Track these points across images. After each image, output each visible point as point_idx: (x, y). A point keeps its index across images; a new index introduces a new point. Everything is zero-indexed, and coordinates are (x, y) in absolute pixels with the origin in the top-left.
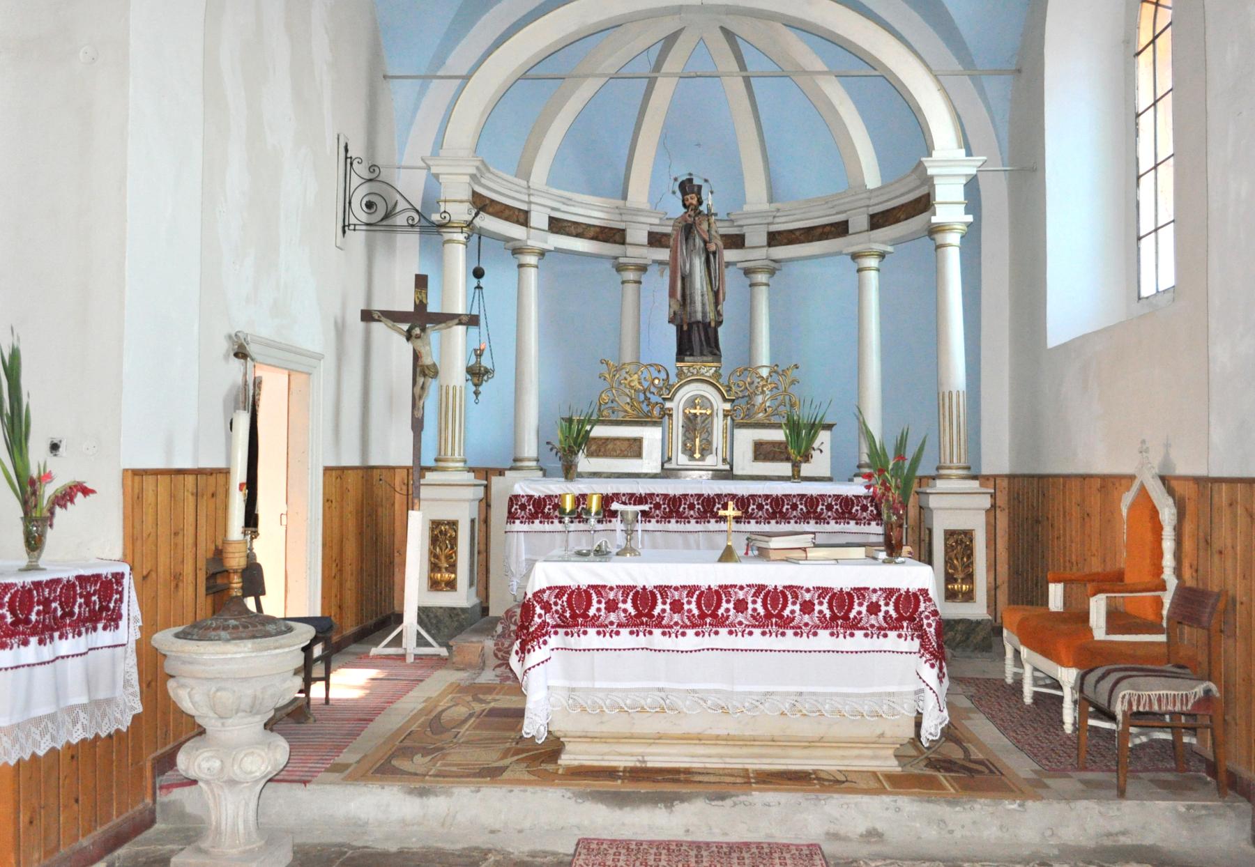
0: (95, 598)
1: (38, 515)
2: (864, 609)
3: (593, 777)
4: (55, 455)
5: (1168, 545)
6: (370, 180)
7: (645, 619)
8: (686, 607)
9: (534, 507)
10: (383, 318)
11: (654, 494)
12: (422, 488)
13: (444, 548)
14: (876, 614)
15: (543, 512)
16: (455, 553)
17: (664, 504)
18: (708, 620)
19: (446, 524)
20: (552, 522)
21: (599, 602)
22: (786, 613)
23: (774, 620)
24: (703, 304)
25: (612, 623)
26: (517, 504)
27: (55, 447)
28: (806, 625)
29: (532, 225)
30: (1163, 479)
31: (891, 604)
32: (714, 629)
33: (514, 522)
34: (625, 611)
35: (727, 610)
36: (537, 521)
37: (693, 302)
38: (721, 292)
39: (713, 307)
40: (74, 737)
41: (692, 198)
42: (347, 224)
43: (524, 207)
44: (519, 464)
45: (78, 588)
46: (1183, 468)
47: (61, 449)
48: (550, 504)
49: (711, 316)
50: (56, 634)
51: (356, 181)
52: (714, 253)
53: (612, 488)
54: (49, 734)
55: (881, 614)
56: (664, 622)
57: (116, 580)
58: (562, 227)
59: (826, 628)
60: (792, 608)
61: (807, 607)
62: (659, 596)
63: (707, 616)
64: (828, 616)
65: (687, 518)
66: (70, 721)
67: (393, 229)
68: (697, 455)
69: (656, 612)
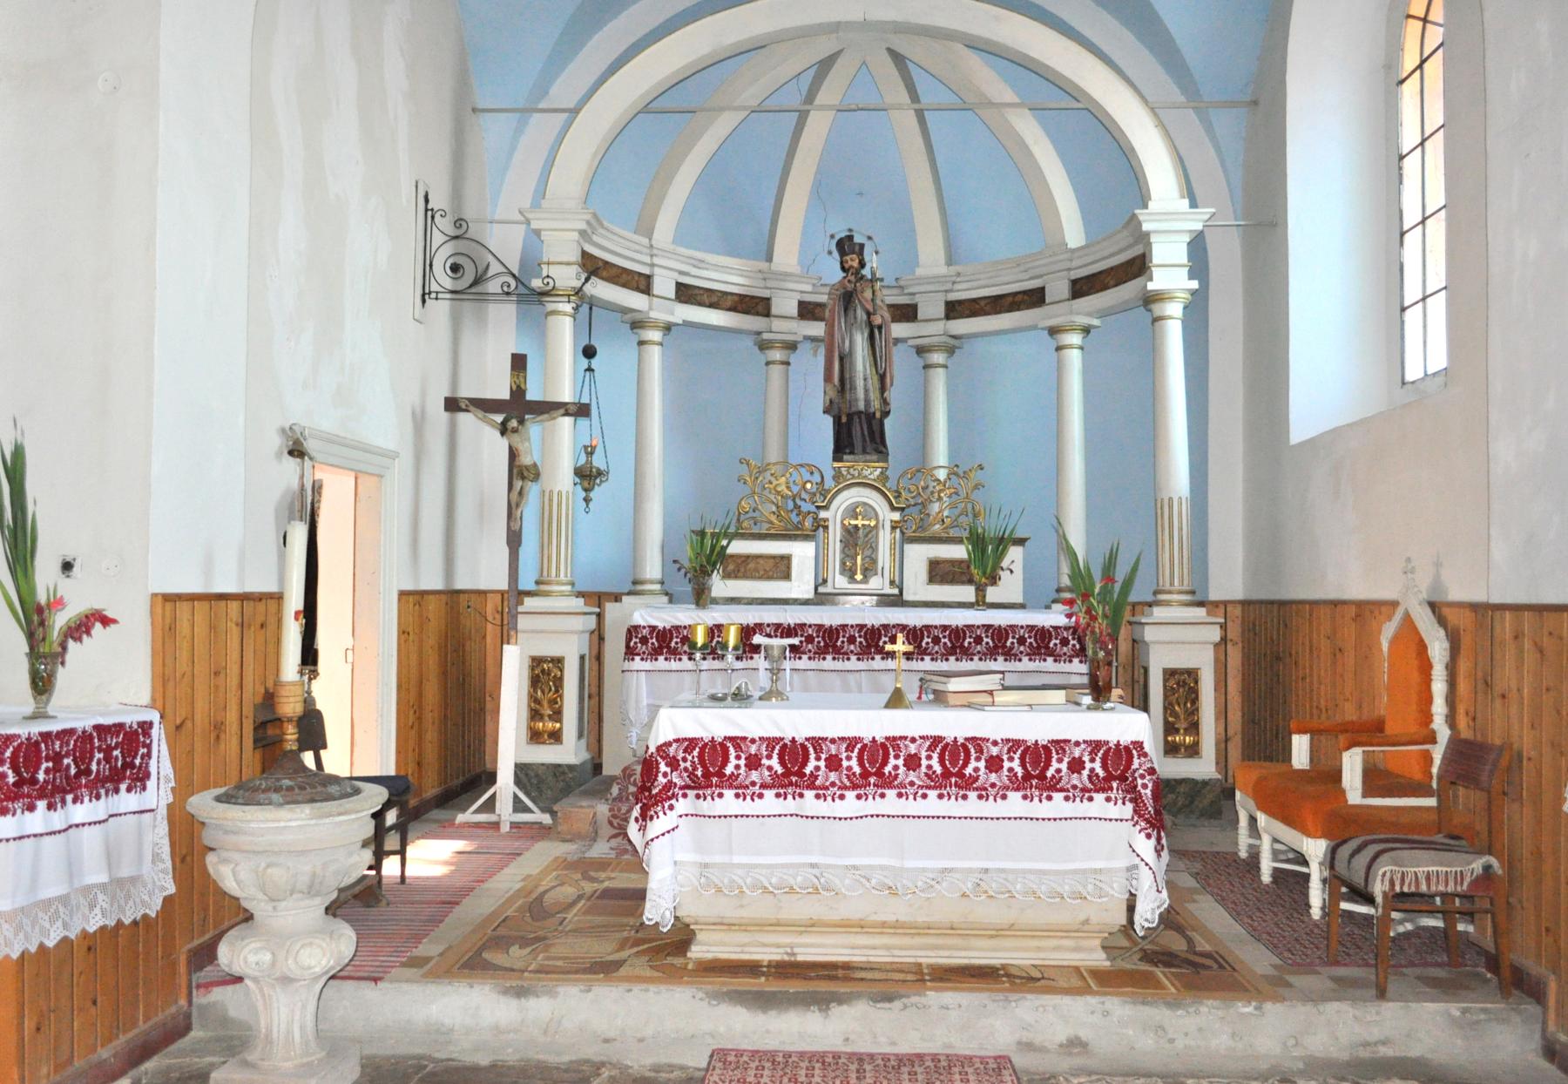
0: (116, 753)
1: (47, 650)
2: (1064, 766)
4: (68, 576)
5: (1439, 687)
6: (456, 237)
7: (794, 779)
8: (845, 763)
9: (657, 640)
10: (471, 408)
11: (805, 625)
12: (519, 616)
13: (546, 691)
14: (1079, 773)
15: (668, 647)
16: (561, 697)
17: (818, 637)
18: (872, 780)
20: (680, 659)
21: (738, 757)
22: (969, 771)
23: (953, 780)
24: (866, 391)
25: (753, 784)
26: (636, 637)
27: (67, 567)
28: (993, 785)
30: (1433, 606)
31: (1098, 760)
32: (880, 791)
33: (633, 659)
34: (770, 768)
35: (896, 768)
36: (661, 658)
37: (853, 388)
38: (888, 375)
39: (878, 394)
40: (91, 924)
41: (852, 260)
42: (427, 291)
43: (646, 270)
44: (639, 587)
45: (96, 740)
46: (1458, 592)
47: (75, 569)
48: (677, 637)
49: (876, 404)
50: (69, 798)
51: (438, 238)
52: (880, 328)
53: (754, 617)
54: (61, 920)
55: (1085, 773)
56: (818, 783)
57: (143, 730)
59: (1017, 789)
60: (976, 765)
61: (994, 764)
62: (811, 750)
63: (870, 774)
64: (1020, 775)
65: (846, 653)
67: (484, 298)
68: (859, 577)
69: (808, 770)
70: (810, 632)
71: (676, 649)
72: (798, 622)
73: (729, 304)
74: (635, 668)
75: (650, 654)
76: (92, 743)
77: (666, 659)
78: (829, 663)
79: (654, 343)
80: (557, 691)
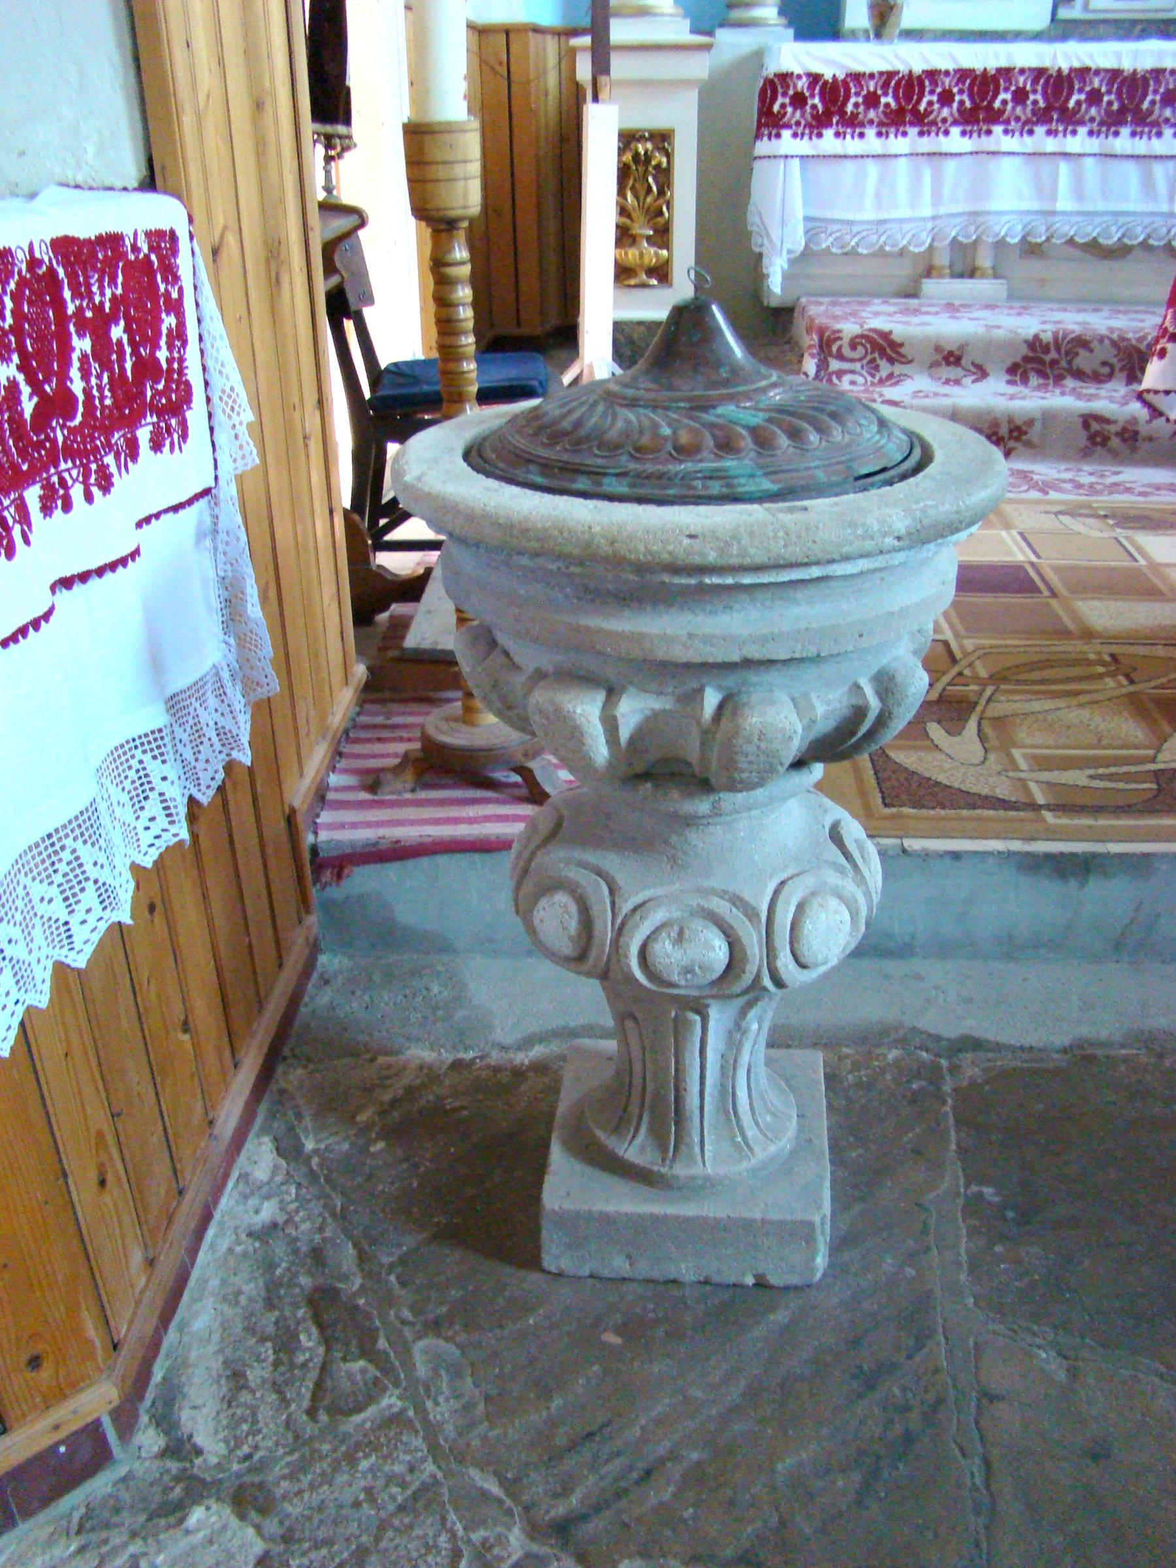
0: (117, 332)
3: (618, 561)
9: (822, 99)
11: (1088, 69)
13: (642, 193)
15: (842, 113)
17: (1109, 92)
19: (647, 140)
20: (862, 135)
26: (784, 94)
33: (778, 136)
36: (829, 133)
45: (67, 294)
48: (857, 94)
50: (33, 495)
53: (996, 56)
57: (161, 259)
65: (1156, 124)
66: (125, 798)
70: (1096, 84)
71: (854, 116)
72: (1077, 65)
74: (782, 152)
75: (808, 125)
76: (847, 90)
77: (837, 135)
78: (1124, 142)
80: (661, 193)
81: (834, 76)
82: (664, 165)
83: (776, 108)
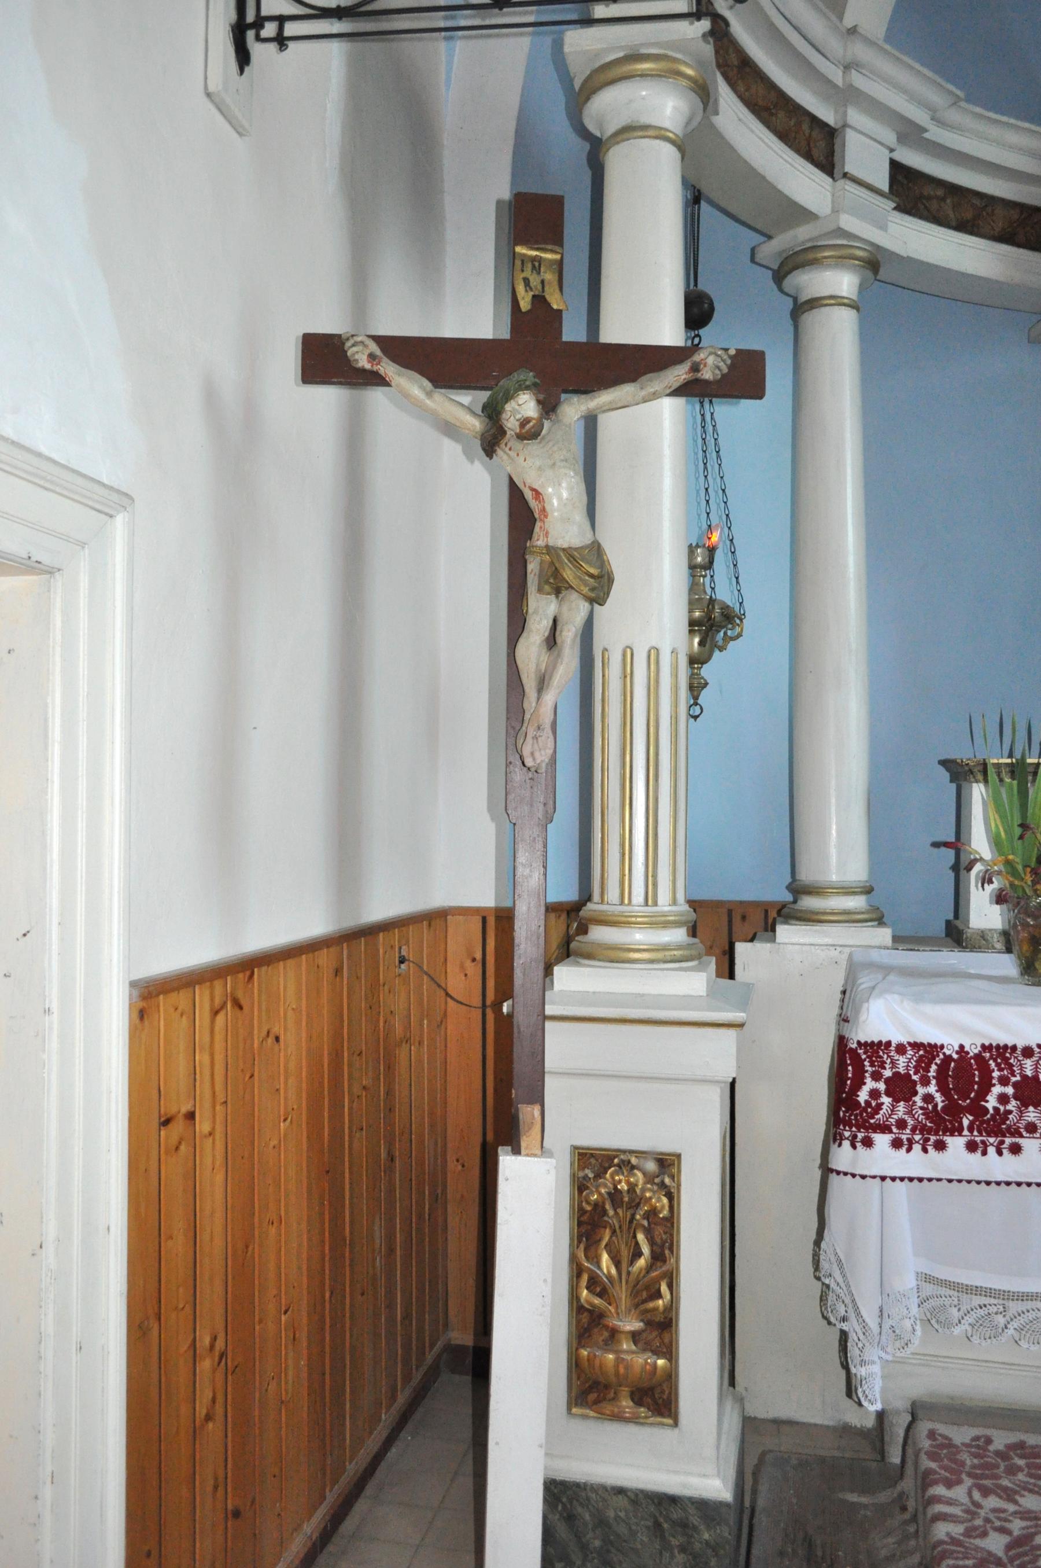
9: (942, 1088)
10: (388, 368)
12: (549, 1025)
13: (625, 1254)
15: (978, 1111)
16: (672, 1279)
26: (876, 1076)
29: (848, 168)
33: (868, 1143)
36: (956, 1144)
42: (250, 17)
43: (826, 114)
44: (809, 903)
48: (1004, 1081)
58: (921, 197)
73: (999, 225)
76: (986, 1074)
79: (837, 301)
81: (962, 1047)
82: (665, 1213)
83: (863, 1096)
